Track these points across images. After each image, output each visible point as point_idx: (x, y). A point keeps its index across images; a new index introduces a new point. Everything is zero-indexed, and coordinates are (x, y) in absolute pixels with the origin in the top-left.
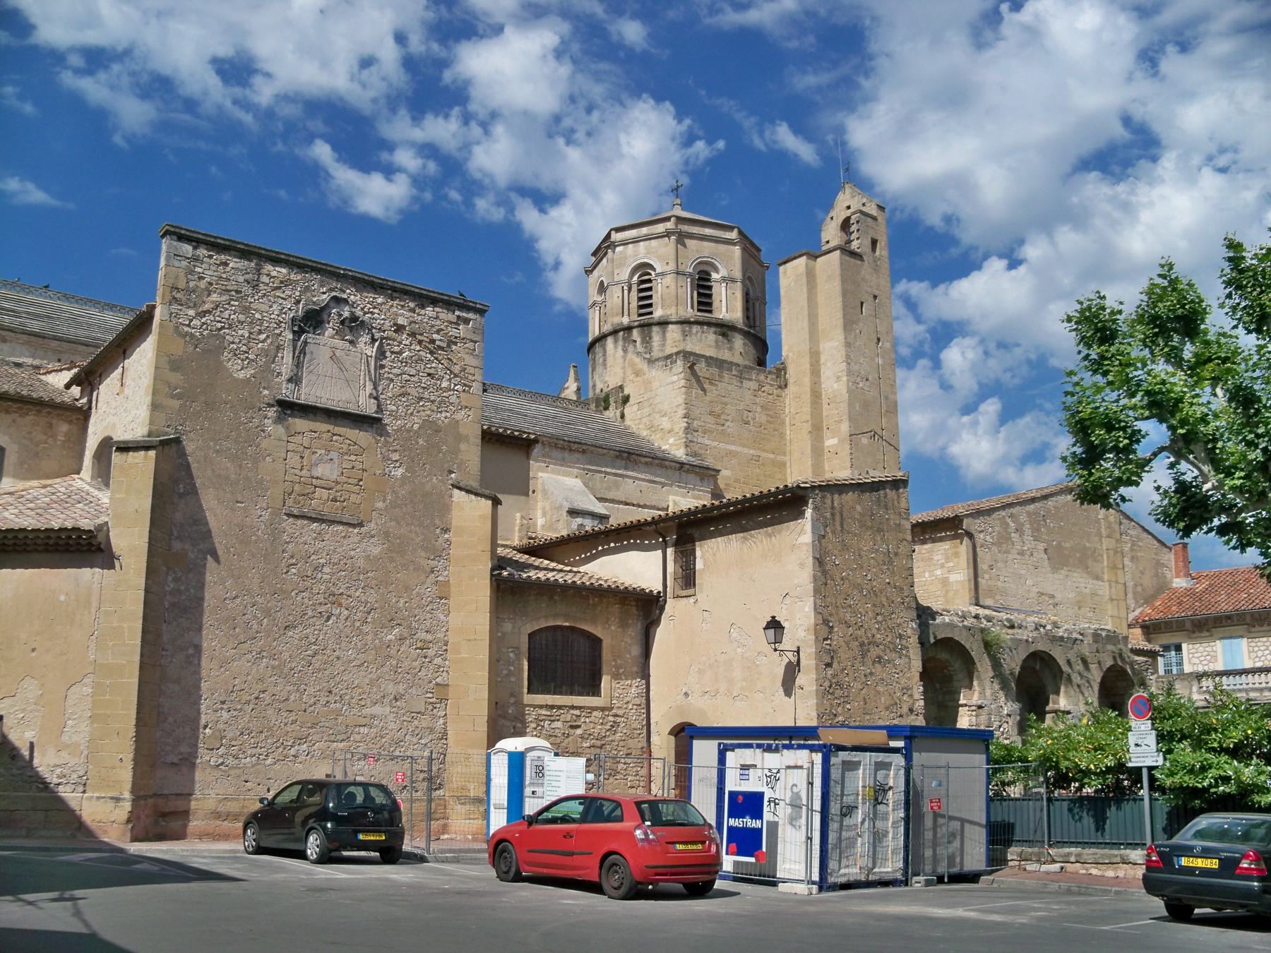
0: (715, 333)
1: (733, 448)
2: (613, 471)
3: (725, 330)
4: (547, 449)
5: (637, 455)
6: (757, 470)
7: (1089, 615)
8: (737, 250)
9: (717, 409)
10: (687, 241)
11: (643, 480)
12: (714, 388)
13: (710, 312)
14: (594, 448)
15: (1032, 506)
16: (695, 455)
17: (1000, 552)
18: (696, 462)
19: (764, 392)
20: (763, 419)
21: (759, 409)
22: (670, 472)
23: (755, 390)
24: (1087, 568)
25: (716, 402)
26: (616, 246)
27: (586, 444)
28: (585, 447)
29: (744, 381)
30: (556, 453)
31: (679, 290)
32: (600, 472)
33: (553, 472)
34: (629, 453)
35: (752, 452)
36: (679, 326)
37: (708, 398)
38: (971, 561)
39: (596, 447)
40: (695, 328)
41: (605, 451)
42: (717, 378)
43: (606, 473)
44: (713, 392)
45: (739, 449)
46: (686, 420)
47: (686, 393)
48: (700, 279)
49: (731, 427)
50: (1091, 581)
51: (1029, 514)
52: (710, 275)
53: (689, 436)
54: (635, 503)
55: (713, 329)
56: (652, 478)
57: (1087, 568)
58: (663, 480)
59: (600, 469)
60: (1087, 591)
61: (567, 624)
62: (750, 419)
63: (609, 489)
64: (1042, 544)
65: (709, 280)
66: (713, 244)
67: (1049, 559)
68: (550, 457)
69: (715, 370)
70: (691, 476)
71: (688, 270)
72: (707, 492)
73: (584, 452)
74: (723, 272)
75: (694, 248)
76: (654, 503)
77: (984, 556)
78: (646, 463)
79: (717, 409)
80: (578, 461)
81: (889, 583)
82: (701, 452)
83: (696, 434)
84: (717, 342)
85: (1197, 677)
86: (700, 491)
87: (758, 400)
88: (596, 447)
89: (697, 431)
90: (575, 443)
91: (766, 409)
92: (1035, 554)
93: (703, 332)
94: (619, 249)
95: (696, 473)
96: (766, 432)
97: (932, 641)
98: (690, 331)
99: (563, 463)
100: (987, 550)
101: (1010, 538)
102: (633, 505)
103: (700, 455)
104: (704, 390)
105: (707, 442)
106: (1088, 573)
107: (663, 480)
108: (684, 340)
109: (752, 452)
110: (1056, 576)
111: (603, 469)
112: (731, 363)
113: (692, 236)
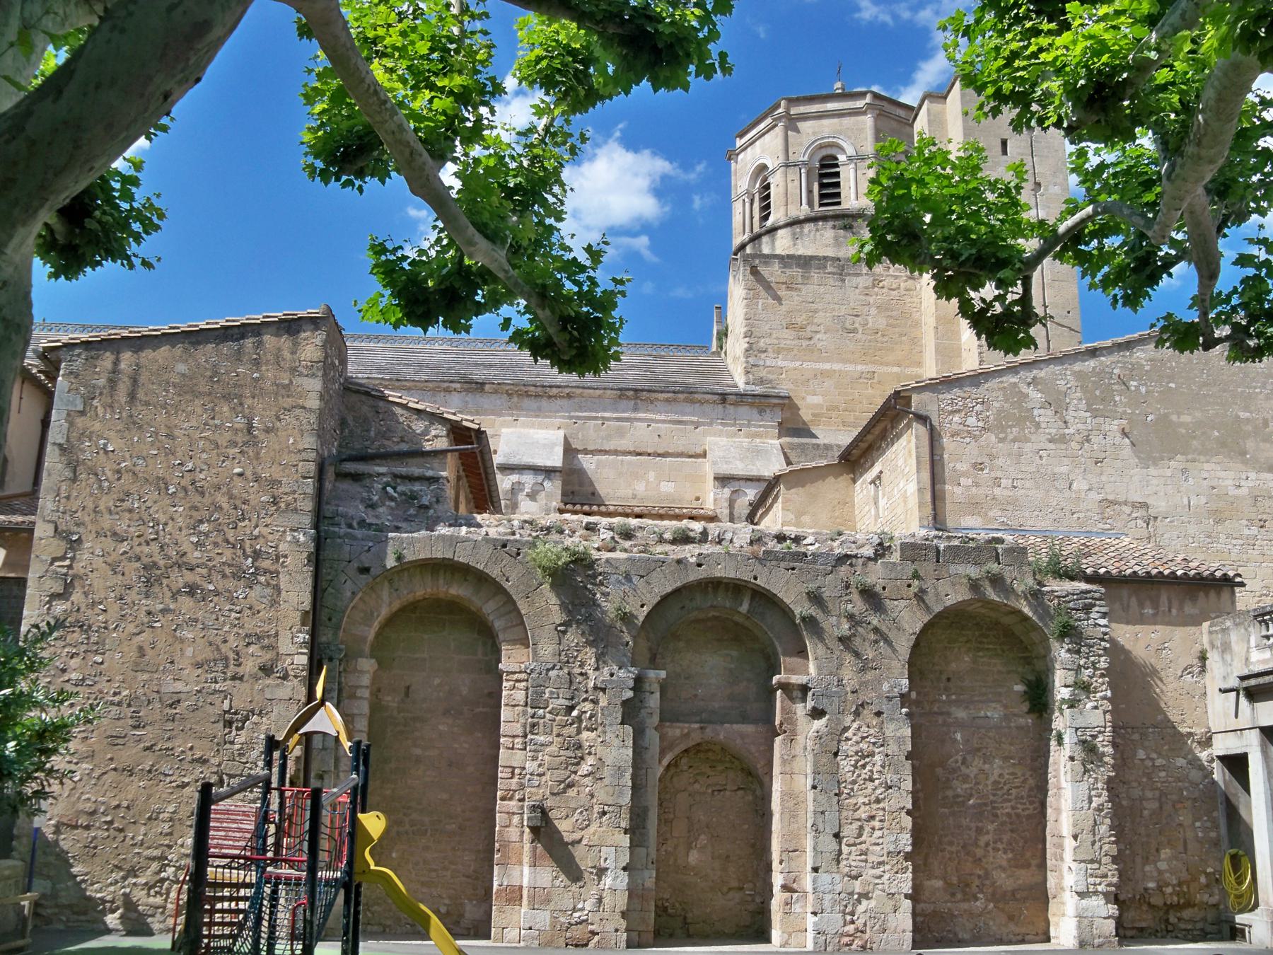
0: (834, 227)
1: (827, 366)
2: (615, 415)
3: (846, 221)
4: (515, 399)
5: (649, 391)
6: (870, 391)
7: (1246, 532)
8: (868, 121)
9: (801, 319)
10: (801, 125)
11: (664, 422)
12: (794, 293)
13: (839, 203)
14: (581, 390)
15: (1092, 363)
16: (761, 381)
17: (1002, 440)
18: (758, 390)
19: (883, 287)
20: (882, 323)
21: (873, 311)
22: (707, 408)
23: (866, 288)
24: (1243, 453)
25: (799, 311)
26: (738, 155)
27: (568, 386)
28: (567, 390)
29: (847, 279)
30: (527, 402)
31: (790, 185)
32: (596, 418)
33: (524, 426)
34: (636, 390)
35: (859, 368)
36: (788, 230)
37: (784, 308)
38: (927, 458)
39: (584, 388)
40: (808, 227)
41: (598, 392)
42: (800, 280)
43: (603, 418)
44: (792, 300)
45: (837, 366)
46: (747, 339)
47: (747, 306)
48: (823, 166)
49: (823, 340)
50: (1252, 475)
51: (1079, 375)
52: (837, 159)
53: (750, 359)
54: (649, 451)
55: (831, 223)
56: (676, 417)
57: (1243, 453)
58: (695, 419)
59: (594, 414)
60: (1244, 491)
61: (12, 575)
62: (857, 325)
63: (608, 437)
64: (1116, 422)
65: (837, 166)
66: (836, 121)
67: (1133, 444)
68: (517, 408)
69: (797, 272)
70: (744, 410)
71: (801, 159)
72: (772, 427)
73: (569, 396)
74: (850, 151)
75: (810, 131)
76: (680, 449)
77: (957, 455)
78: (667, 400)
79: (799, 320)
80: (562, 409)
81: (240, 475)
82: (771, 377)
83: (763, 356)
84: (836, 238)
85: (1255, 617)
86: (760, 426)
87: (871, 300)
88: (584, 388)
89: (765, 352)
90: (551, 387)
91: (887, 309)
92: (1094, 439)
93: (817, 230)
94: (740, 157)
95: (751, 405)
96: (885, 339)
97: (391, 562)
98: (802, 232)
99: (539, 413)
100: (968, 440)
101: (1031, 418)
102: (649, 455)
103: (771, 381)
104: (778, 299)
105: (780, 363)
106: (1245, 462)
107: (695, 419)
108: (795, 245)
109: (859, 368)
110: (1153, 471)
111: (599, 415)
112: (825, 258)
113: (805, 117)
